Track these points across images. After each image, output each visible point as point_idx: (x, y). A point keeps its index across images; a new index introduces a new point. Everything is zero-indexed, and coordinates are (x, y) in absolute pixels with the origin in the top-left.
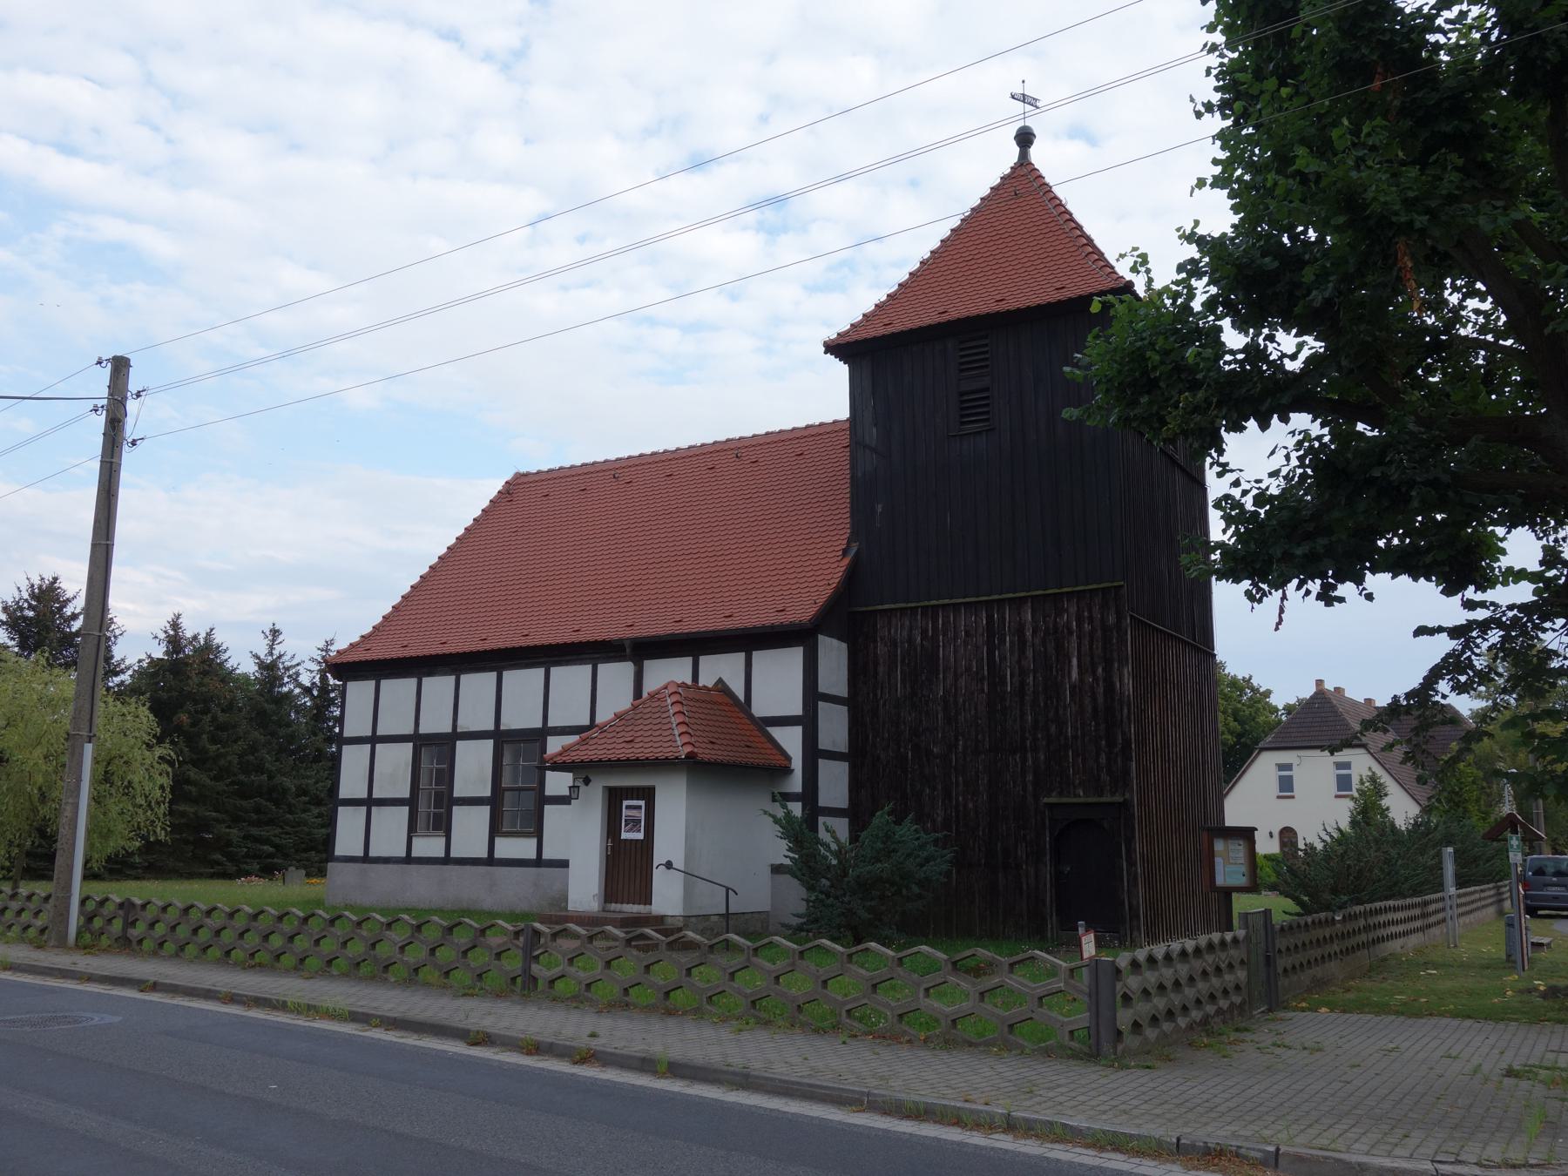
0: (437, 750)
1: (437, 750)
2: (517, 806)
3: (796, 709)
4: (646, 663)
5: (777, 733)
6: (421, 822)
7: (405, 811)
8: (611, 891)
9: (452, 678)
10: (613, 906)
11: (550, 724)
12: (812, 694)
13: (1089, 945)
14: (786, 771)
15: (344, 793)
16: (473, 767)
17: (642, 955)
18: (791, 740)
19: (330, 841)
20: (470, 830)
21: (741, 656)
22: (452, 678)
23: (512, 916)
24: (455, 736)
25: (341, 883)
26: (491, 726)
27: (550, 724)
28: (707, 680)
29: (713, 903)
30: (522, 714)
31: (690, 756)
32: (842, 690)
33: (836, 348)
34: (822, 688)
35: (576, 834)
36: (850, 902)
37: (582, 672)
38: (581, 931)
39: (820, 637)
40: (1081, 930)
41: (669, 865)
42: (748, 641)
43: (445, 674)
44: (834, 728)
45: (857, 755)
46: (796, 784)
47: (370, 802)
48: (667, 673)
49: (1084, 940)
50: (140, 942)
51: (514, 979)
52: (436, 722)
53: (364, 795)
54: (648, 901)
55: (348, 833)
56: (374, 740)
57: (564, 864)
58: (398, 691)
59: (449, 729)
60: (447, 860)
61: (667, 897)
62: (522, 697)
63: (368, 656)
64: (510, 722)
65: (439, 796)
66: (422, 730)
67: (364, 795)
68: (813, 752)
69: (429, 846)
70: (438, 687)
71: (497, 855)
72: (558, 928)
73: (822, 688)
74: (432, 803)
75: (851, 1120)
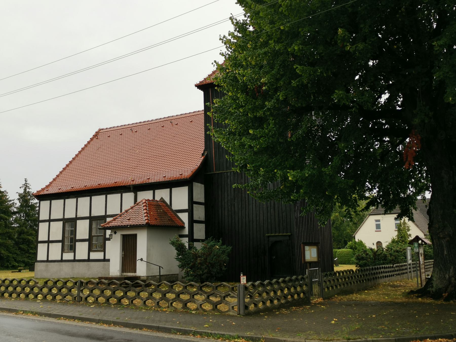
0: (70, 223)
1: (70, 223)
2: (96, 242)
3: (186, 207)
4: (138, 193)
5: (180, 215)
6: (66, 248)
7: (87, 243)
8: (124, 268)
10: (125, 274)
11: (108, 214)
12: (191, 202)
13: (243, 280)
14: (183, 227)
15: (40, 239)
16: (83, 229)
17: (124, 289)
18: (184, 217)
19: (36, 254)
20: (82, 250)
21: (169, 190)
22: (49, 201)
24: (77, 219)
25: (41, 272)
27: (108, 214)
28: (157, 198)
29: (156, 272)
30: (98, 211)
31: (147, 223)
32: (202, 200)
33: (200, 86)
34: (195, 200)
35: (114, 249)
36: (202, 271)
38: (106, 281)
39: (194, 183)
40: (242, 275)
41: (142, 260)
42: (170, 184)
44: (200, 213)
45: (209, 222)
46: (186, 232)
47: (49, 242)
49: (242, 278)
51: (75, 298)
52: (70, 214)
53: (47, 240)
54: (135, 272)
55: (41, 254)
56: (50, 221)
57: (108, 260)
58: (57, 204)
59: (74, 216)
60: (74, 260)
61: (141, 270)
62: (98, 205)
63: (47, 193)
64: (94, 214)
65: (72, 239)
66: (66, 217)
67: (47, 240)
68: (192, 221)
69: (68, 256)
70: (71, 202)
71: (91, 258)
72: (110, 282)
73: (195, 200)
74: (69, 242)
75: (151, 334)
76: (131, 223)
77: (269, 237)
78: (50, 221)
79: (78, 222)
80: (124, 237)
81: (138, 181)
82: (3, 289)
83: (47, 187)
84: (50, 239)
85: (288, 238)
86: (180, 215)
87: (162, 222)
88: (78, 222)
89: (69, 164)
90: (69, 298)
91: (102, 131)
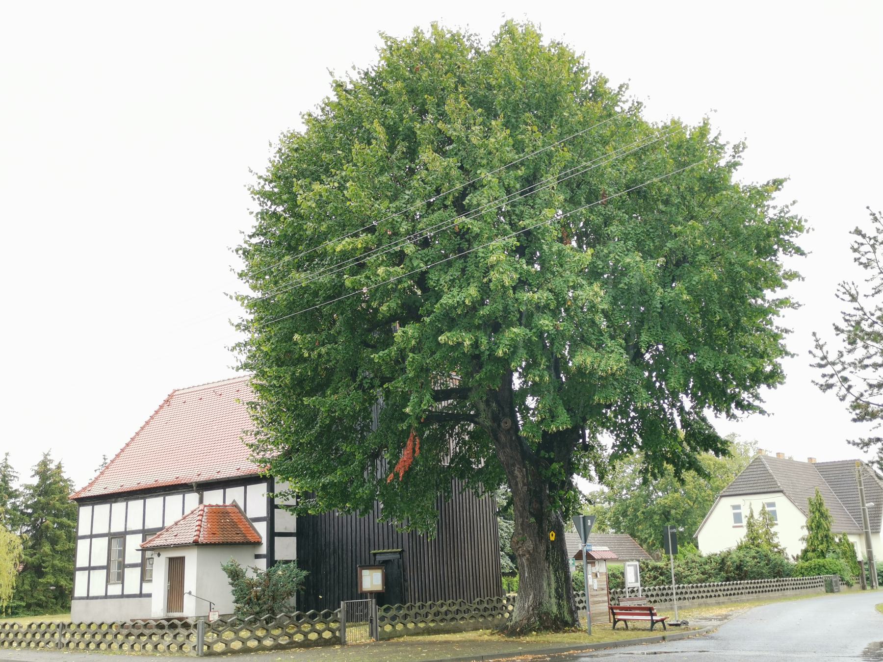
1: (117, 538)
5: (256, 525)
7: (139, 570)
8: (170, 607)
9: (125, 503)
12: (272, 506)
14: (259, 544)
15: (78, 565)
18: (262, 528)
19: (72, 591)
23: (156, 620)
25: (79, 613)
26: (141, 528)
37: (160, 500)
41: (190, 593)
43: (137, 499)
44: (286, 521)
46: (263, 550)
48: (214, 498)
50: (68, 644)
52: (117, 527)
53: (87, 565)
57: (149, 595)
59: (123, 530)
60: (123, 596)
61: (190, 609)
64: (150, 525)
65: (119, 563)
68: (272, 534)
69: (115, 590)
70: (154, 503)
74: (116, 568)
76: (177, 541)
77: (375, 554)
78: (91, 536)
79: (128, 537)
80: (171, 560)
81: (204, 478)
82: (3, 635)
83: (91, 484)
84: (92, 565)
85: (398, 556)
86: (257, 525)
87: (227, 535)
88: (128, 537)
89: (125, 448)
90: (52, 644)
91: (177, 393)
